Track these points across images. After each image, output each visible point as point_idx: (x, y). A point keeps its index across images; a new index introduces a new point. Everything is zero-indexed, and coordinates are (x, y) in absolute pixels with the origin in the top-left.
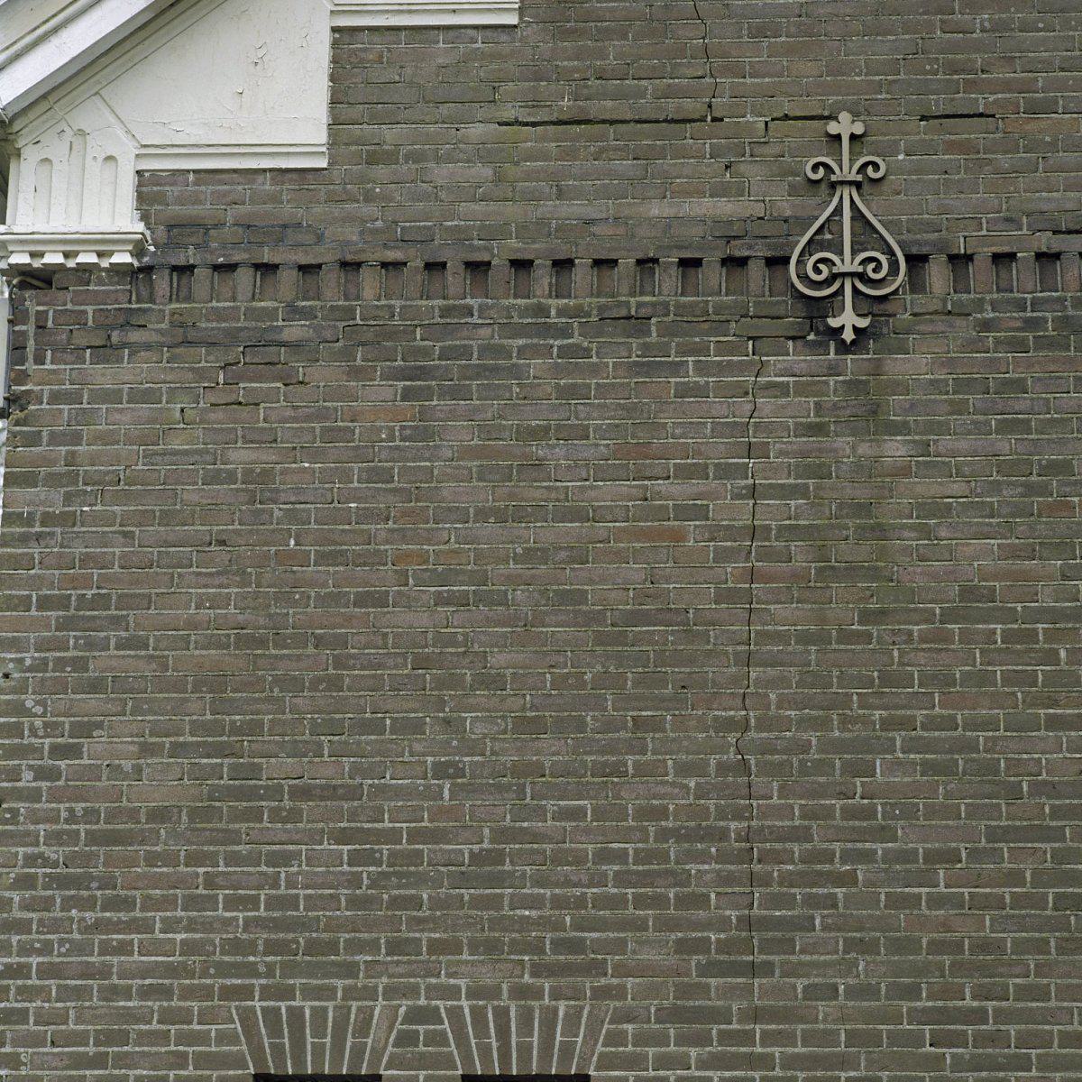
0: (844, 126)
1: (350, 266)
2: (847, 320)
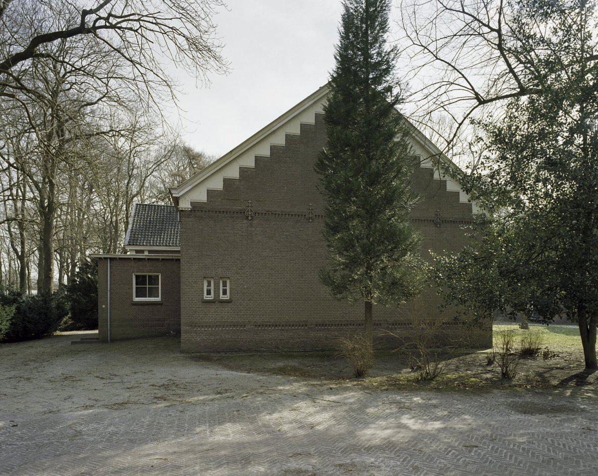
0: (250, 201)
1: (209, 211)
2: (250, 218)
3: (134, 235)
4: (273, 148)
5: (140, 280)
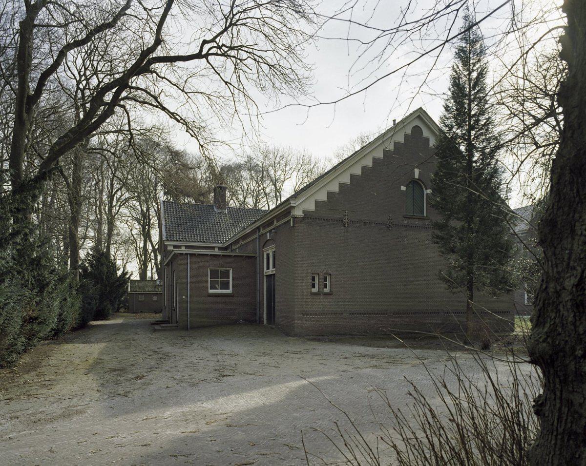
3: (169, 231)
4: (363, 168)
5: (214, 274)
